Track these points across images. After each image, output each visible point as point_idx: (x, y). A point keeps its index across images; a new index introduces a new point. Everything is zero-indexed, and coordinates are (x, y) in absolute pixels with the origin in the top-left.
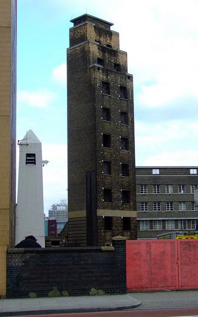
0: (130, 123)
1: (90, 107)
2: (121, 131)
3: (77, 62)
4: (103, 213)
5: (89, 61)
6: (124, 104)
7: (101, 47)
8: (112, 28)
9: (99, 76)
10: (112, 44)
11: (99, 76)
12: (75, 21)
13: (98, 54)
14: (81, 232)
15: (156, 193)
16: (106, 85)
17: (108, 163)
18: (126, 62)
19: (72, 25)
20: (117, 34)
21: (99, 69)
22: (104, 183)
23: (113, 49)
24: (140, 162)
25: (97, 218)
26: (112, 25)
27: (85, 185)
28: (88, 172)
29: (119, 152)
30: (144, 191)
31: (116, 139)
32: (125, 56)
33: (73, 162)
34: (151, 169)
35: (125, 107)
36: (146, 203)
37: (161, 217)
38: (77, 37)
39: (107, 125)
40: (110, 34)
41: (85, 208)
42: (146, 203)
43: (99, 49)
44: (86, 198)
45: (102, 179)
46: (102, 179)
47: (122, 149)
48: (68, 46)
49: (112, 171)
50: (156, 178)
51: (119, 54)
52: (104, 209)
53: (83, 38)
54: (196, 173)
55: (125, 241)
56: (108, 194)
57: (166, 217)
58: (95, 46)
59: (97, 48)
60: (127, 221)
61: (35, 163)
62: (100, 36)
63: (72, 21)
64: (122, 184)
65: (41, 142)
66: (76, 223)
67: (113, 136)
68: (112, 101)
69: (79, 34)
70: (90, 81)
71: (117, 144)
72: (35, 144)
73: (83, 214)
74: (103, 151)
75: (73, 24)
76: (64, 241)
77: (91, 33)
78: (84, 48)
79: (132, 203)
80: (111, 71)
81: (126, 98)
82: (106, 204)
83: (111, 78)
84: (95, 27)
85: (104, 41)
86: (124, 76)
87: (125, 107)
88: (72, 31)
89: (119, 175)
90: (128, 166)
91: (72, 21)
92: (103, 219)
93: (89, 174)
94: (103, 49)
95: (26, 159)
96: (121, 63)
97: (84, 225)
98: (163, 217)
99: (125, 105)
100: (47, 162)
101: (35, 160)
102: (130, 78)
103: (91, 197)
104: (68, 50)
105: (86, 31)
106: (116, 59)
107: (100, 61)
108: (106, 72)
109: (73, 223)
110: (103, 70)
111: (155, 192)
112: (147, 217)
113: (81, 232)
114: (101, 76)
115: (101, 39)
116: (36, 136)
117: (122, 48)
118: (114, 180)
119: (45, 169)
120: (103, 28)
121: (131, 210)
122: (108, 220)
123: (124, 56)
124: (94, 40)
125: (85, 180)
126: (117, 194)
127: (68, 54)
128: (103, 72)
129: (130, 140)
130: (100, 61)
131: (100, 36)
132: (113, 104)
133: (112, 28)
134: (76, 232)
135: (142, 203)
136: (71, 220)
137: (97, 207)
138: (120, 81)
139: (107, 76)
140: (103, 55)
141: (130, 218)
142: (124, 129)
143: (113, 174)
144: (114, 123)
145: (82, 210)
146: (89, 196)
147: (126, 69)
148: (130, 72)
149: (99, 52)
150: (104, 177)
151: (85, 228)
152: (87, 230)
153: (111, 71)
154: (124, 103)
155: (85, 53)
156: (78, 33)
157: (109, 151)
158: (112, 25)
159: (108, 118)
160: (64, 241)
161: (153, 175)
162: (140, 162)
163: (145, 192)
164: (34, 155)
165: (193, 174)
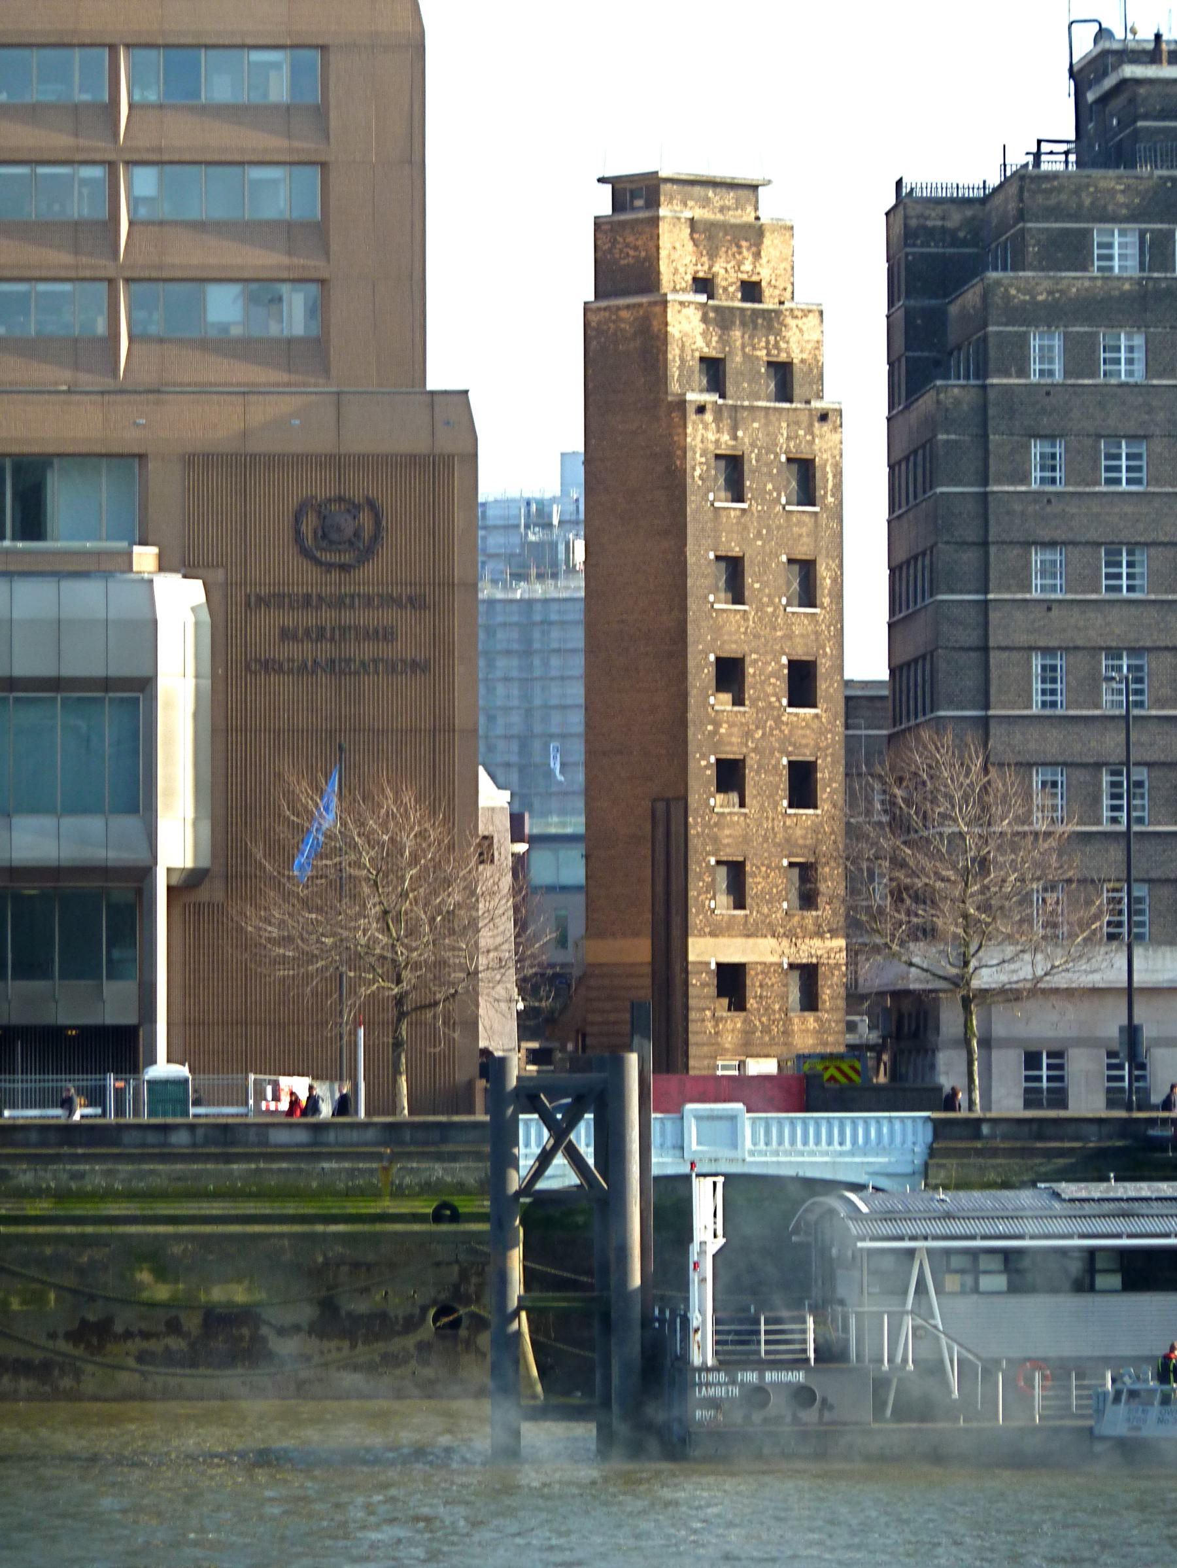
1: (670, 557)
2: (789, 636)
13: (700, 343)
27: (649, 845)
29: (778, 720)
39: (813, 949)
43: (705, 319)
45: (711, 828)
46: (711, 828)
54: (581, 830)
59: (699, 315)
62: (713, 256)
63: (847, 1046)
64: (720, 628)
67: (756, 661)
69: (632, 253)
71: (770, 690)
76: (570, 1047)
87: (805, 539)
89: (776, 805)
91: (847, 1046)
93: (661, 806)
99: (804, 530)
106: (777, 342)
110: (718, 411)
114: (711, 436)
125: (648, 827)
128: (718, 419)
132: (759, 535)
137: (1139, 324)
138: (789, 438)
144: (760, 609)
145: (636, 934)
146: (660, 889)
149: (704, 334)
150: (715, 819)
154: (800, 524)
156: (628, 245)
159: (736, 591)
160: (570, 1047)
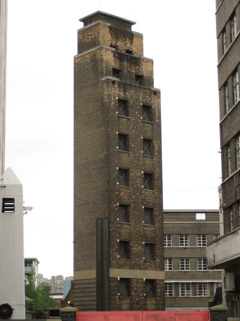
0: (156, 154)
1: (103, 133)
2: (144, 164)
3: (86, 73)
4: (117, 273)
5: (102, 73)
6: (148, 128)
7: (118, 53)
8: (134, 29)
9: (116, 93)
10: (134, 49)
11: (116, 93)
12: (86, 20)
13: (113, 63)
14: (89, 298)
15: (202, 246)
16: (123, 103)
17: (125, 207)
18: (152, 72)
19: (81, 25)
20: (140, 36)
21: (114, 82)
22: (119, 233)
23: (135, 55)
24: (169, 204)
25: (111, 280)
26: (133, 23)
28: (97, 219)
30: (184, 243)
31: (137, 175)
32: (151, 65)
33: (80, 205)
34: (194, 213)
35: (150, 133)
36: (188, 259)
37: (208, 279)
38: (86, 41)
40: (131, 36)
41: (95, 267)
42: (188, 259)
43: (114, 56)
44: (95, 253)
47: (145, 188)
48: (76, 53)
49: (131, 217)
50: (201, 224)
51: (142, 63)
52: (118, 267)
53: (95, 43)
55: (75, 312)
56: (125, 245)
57: (215, 279)
58: (109, 52)
59: (112, 55)
60: (151, 282)
61: (13, 210)
62: (117, 39)
63: (82, 20)
65: (22, 183)
66: (84, 286)
67: (133, 171)
68: (132, 125)
69: (90, 38)
70: (102, 99)
71: (138, 182)
72: (14, 186)
73: (92, 274)
74: (118, 191)
75: (83, 23)
77: (105, 35)
78: (95, 56)
79: (158, 260)
80: (131, 85)
81: (151, 120)
82: (123, 261)
83: (130, 94)
84: (110, 28)
85: (122, 45)
86: (148, 91)
88: (81, 33)
89: (141, 222)
90: (154, 210)
91: (82, 20)
92: (117, 281)
94: (119, 56)
95: (14, 202)
96: (145, 74)
97: (93, 290)
98: (212, 279)
100: (31, 209)
101: (13, 206)
102: (157, 93)
103: (102, 252)
104: (75, 58)
105: (99, 33)
106: (138, 70)
107: (116, 72)
108: (124, 86)
109: (81, 286)
110: (119, 84)
111: (200, 245)
112: (190, 279)
113: (89, 298)
115: (119, 44)
116: (15, 176)
117: (147, 54)
118: (135, 228)
119: (28, 219)
120: (121, 28)
121: (156, 270)
122: (126, 281)
123: (149, 64)
124: (109, 44)
126: (137, 248)
127: (75, 63)
129: (156, 176)
130: (116, 72)
131: (117, 39)
133: (134, 29)
134: (83, 299)
135: (182, 259)
136: (74, 283)
137: (109, 266)
138: (143, 98)
139: (125, 91)
140: (120, 64)
141: (130, 279)
142: (148, 161)
143: (132, 222)
147: (151, 82)
148: (156, 85)
149: (114, 61)
150: (119, 225)
151: (95, 294)
152: (97, 296)
153: (131, 85)
155: (95, 62)
157: (128, 191)
158: (133, 23)
161: (196, 221)
162: (169, 204)
163: (186, 245)
164: (12, 200)
165: (201, 220)
